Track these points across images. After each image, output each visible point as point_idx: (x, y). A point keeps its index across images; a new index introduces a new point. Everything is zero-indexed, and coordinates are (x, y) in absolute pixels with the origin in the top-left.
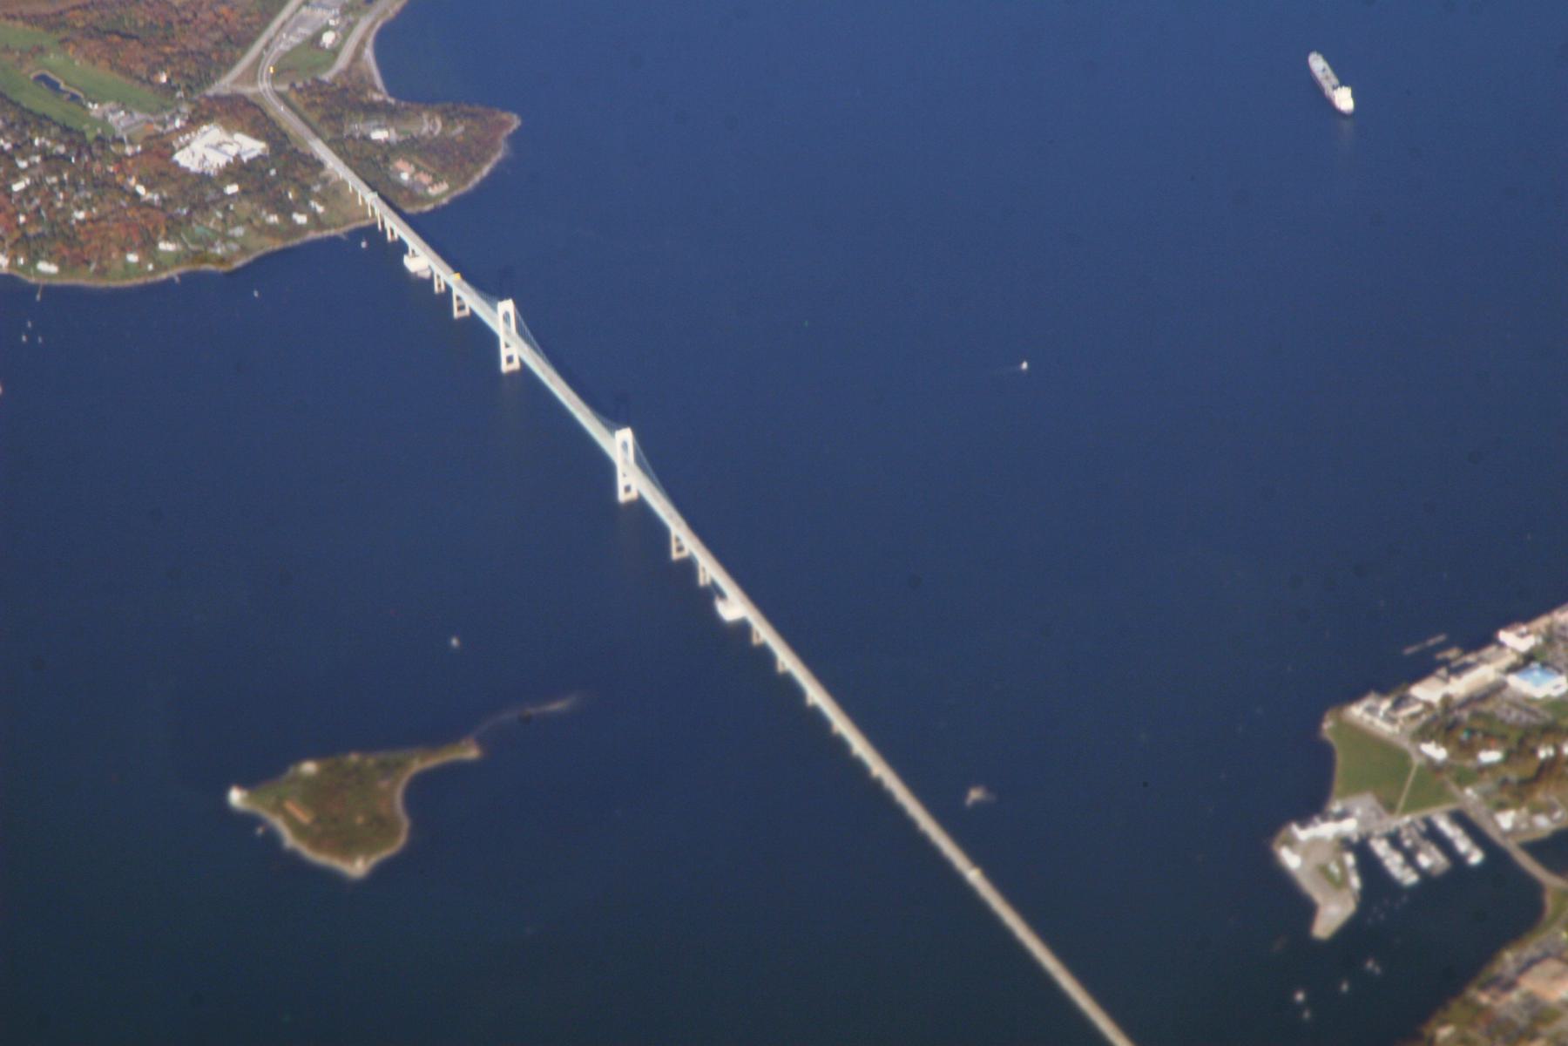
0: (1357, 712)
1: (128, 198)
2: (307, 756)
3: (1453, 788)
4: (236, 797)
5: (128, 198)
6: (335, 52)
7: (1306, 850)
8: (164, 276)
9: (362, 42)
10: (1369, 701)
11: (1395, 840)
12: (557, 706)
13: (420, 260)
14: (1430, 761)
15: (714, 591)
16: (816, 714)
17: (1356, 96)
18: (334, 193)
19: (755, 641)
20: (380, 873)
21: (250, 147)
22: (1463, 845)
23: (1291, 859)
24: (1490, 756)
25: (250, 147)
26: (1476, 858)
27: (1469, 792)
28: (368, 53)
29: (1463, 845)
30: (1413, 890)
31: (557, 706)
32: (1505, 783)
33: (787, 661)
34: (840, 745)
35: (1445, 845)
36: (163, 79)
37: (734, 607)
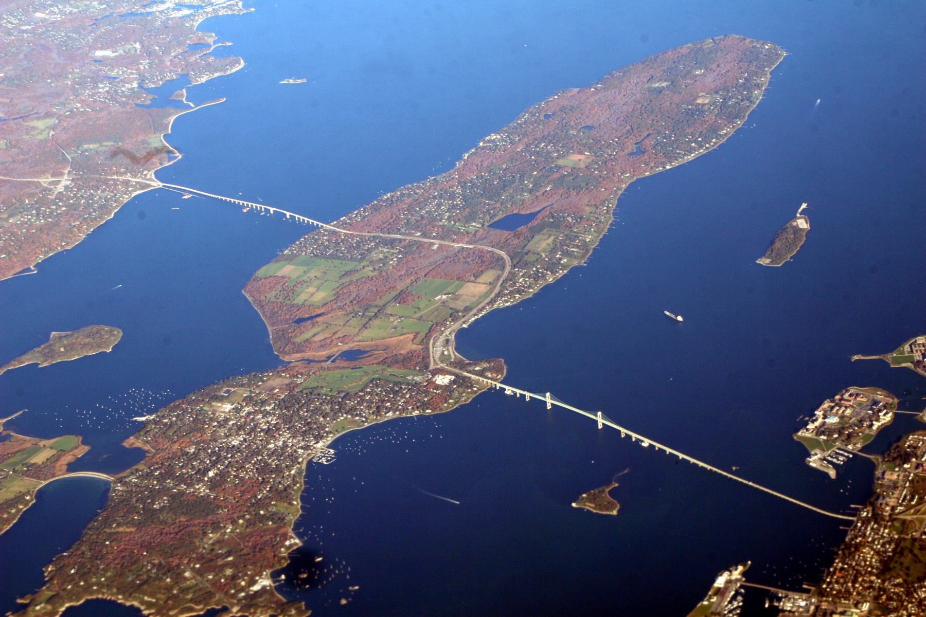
0: (800, 433)
1: (105, 588)
2: (584, 493)
3: (833, 444)
4: (574, 505)
5: (105, 588)
6: (449, 355)
7: (815, 461)
8: (455, 407)
9: (453, 352)
10: (801, 431)
11: (830, 456)
12: (626, 472)
13: (509, 391)
14: (824, 439)
15: (638, 441)
16: (702, 467)
17: (682, 317)
18: (477, 382)
19: (691, 462)
20: (619, 511)
21: (453, 378)
22: (846, 454)
23: (813, 465)
24: (836, 436)
25: (453, 378)
26: (851, 456)
27: (837, 444)
28: (456, 354)
29: (846, 454)
30: (843, 465)
31: (626, 472)
32: (843, 441)
33: (692, 460)
34: (721, 474)
35: (842, 455)
36: (418, 368)
37: (646, 443)
